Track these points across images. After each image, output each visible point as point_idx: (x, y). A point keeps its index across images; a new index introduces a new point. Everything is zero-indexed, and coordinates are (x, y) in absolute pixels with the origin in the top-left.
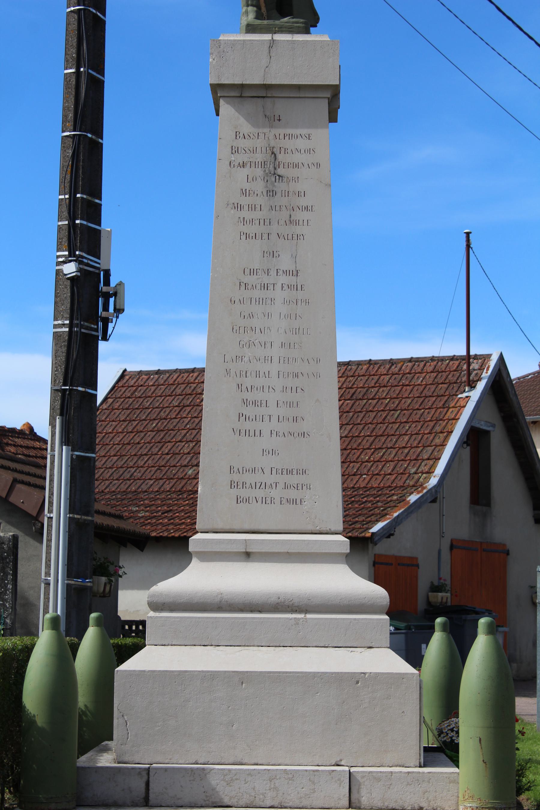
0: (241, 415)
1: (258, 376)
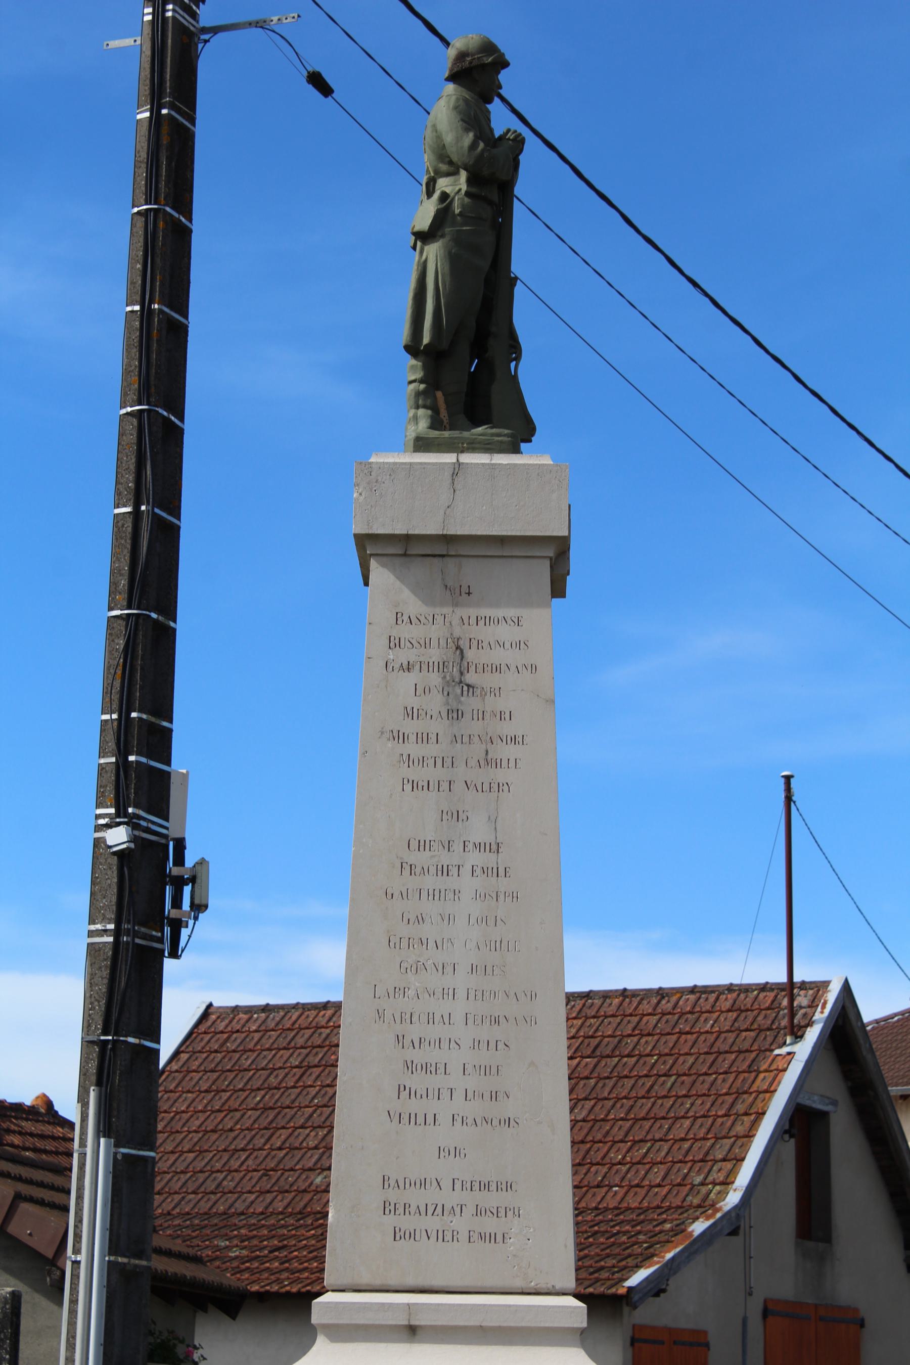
0: (402, 1088)
1: (431, 1021)
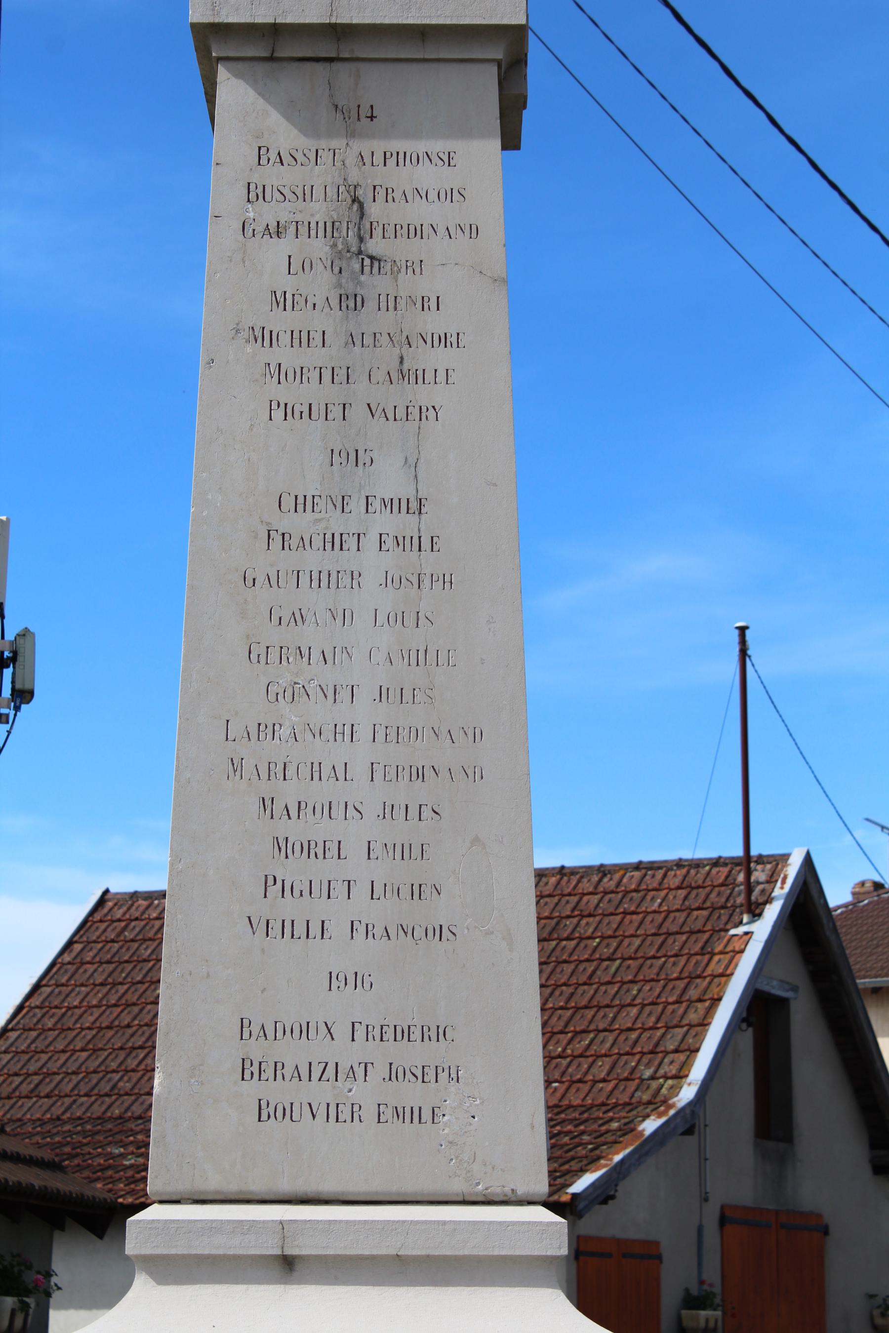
0: (271, 881)
1: (316, 776)
